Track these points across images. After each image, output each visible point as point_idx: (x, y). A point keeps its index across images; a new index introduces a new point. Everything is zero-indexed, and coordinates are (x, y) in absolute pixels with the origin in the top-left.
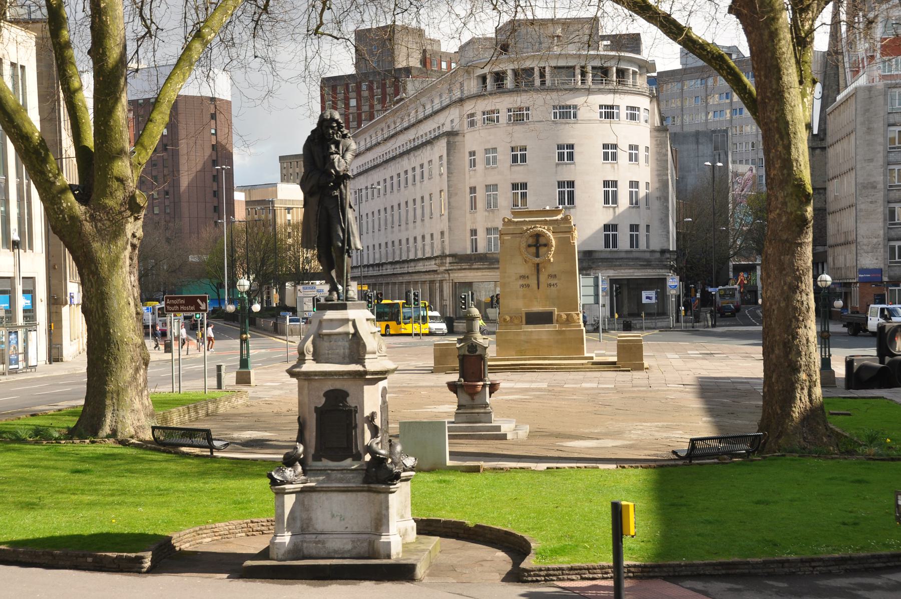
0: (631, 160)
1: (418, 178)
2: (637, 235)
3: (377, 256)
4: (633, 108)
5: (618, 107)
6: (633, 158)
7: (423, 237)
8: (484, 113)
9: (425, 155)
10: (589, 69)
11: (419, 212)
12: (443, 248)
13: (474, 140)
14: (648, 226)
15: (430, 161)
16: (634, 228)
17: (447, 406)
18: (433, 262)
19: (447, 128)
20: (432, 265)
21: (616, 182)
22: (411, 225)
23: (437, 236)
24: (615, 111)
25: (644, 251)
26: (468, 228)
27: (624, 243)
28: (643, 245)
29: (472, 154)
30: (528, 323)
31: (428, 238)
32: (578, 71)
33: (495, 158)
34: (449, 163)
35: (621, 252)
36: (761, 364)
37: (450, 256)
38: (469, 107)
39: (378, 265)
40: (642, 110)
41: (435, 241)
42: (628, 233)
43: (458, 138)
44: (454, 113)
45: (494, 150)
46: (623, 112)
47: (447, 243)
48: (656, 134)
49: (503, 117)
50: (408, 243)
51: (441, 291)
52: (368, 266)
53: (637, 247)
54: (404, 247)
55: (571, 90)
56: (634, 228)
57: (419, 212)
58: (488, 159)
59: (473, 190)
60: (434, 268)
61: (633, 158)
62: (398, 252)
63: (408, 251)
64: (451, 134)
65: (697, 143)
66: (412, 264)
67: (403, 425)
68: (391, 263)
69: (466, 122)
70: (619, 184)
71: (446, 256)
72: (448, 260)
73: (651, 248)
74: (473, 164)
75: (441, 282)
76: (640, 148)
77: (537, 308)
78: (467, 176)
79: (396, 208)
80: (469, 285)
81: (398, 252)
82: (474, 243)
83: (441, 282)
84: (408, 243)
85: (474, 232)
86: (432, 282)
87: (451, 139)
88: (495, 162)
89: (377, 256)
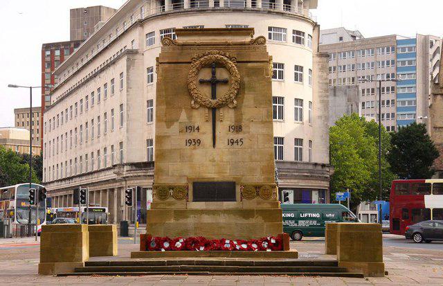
0: (296, 79)
1: (102, 97)
2: (301, 149)
3: (68, 171)
4: (298, 32)
5: (285, 30)
6: (298, 78)
7: (105, 149)
11: (102, 127)
12: (122, 158)
14: (310, 141)
15: (112, 81)
16: (299, 141)
18: (112, 171)
19: (129, 47)
20: (110, 175)
21: (283, 98)
22: (96, 140)
23: (117, 147)
24: (283, 33)
25: (307, 164)
27: (289, 155)
28: (306, 159)
30: (197, 198)
31: (109, 149)
34: (128, 79)
35: (287, 162)
36: (384, 248)
37: (126, 164)
38: (149, 28)
40: (306, 35)
42: (293, 146)
43: (137, 57)
46: (290, 35)
47: (124, 153)
48: (318, 59)
50: (92, 157)
51: (119, 198)
52: (61, 180)
53: (301, 160)
55: (241, 11)
56: (299, 141)
57: (102, 127)
60: (114, 176)
61: (298, 78)
62: (84, 165)
63: (93, 164)
64: (131, 53)
65: (335, 95)
66: (96, 175)
69: (145, 40)
70: (285, 100)
71: (124, 165)
72: (126, 168)
73: (314, 161)
75: (120, 189)
76: (304, 69)
78: (145, 91)
80: (328, 253)
81: (84, 165)
83: (112, 190)
84: (92, 157)
86: (112, 190)
87: (131, 57)
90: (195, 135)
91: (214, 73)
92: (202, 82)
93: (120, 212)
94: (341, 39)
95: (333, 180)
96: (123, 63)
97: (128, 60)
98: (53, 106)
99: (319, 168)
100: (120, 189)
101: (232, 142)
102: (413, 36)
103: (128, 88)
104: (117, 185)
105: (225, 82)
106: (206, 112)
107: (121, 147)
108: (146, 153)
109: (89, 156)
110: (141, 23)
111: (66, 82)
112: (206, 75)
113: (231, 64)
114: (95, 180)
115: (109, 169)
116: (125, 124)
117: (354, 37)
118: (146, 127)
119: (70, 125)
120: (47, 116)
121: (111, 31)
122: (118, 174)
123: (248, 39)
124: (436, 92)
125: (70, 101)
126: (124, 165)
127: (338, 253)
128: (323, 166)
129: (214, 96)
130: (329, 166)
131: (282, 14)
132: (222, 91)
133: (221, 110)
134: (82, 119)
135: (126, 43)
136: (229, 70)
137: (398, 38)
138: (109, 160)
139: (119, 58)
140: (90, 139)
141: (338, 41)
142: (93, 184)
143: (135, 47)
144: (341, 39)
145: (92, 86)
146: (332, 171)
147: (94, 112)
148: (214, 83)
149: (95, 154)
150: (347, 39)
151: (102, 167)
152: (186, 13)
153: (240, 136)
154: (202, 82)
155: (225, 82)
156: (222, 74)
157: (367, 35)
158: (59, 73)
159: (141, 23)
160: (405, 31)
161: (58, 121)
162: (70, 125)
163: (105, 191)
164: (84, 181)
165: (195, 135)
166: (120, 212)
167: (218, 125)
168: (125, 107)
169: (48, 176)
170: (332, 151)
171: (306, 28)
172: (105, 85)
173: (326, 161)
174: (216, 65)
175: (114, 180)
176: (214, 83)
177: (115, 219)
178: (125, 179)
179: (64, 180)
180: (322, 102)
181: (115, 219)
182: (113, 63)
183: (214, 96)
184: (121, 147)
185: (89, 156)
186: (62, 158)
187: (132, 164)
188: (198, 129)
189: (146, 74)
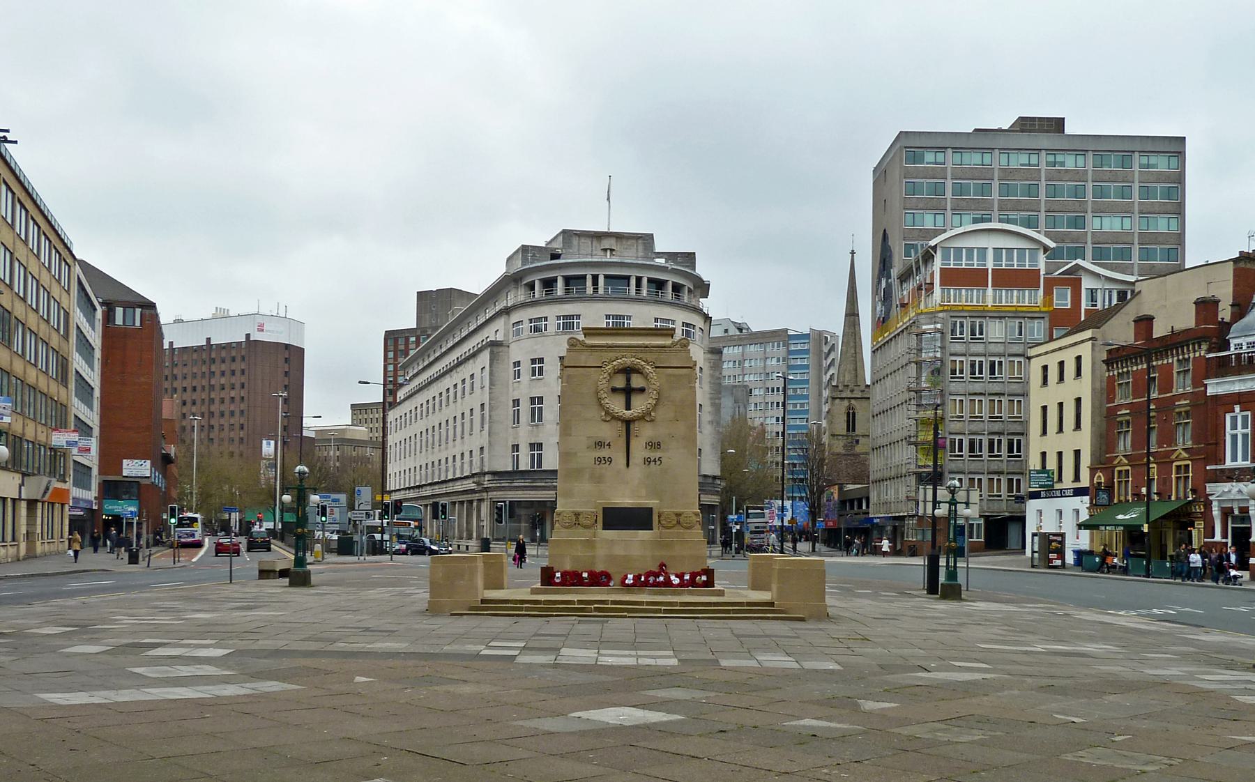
3: (418, 478)
4: (688, 325)
5: (673, 322)
8: (531, 321)
9: (465, 372)
10: (645, 281)
13: (521, 351)
15: (472, 376)
17: (1088, 618)
18: (471, 481)
19: (492, 338)
23: (476, 453)
26: (510, 444)
29: (517, 364)
30: (607, 526)
31: (467, 455)
32: (633, 282)
33: (541, 369)
34: (491, 374)
38: (515, 317)
39: (418, 487)
41: (474, 459)
43: (501, 349)
44: (500, 324)
45: (541, 360)
47: (486, 460)
48: (709, 356)
49: (552, 325)
54: (443, 467)
58: (534, 370)
59: (516, 402)
60: (473, 486)
62: (437, 472)
63: (447, 471)
64: (495, 344)
67: (564, 574)
68: (430, 484)
71: (485, 474)
74: (518, 375)
75: (480, 501)
77: (624, 499)
79: (437, 428)
81: (437, 472)
82: (516, 460)
83: (471, 502)
85: (516, 448)
86: (471, 502)
87: (495, 349)
88: (541, 373)
89: (418, 478)
90: (604, 453)
91: (628, 380)
92: (614, 390)
93: (480, 528)
94: (726, 331)
95: (727, 493)
96: (485, 357)
97: (492, 353)
98: (400, 403)
99: (710, 480)
100: (480, 501)
101: (648, 461)
102: (807, 331)
103: (492, 384)
104: (477, 496)
105: (642, 390)
106: (620, 427)
107: (482, 453)
108: (510, 460)
109: (443, 462)
110: (507, 311)
111: (415, 376)
112: (620, 382)
113: (649, 369)
114: (450, 490)
115: (467, 477)
116: (486, 427)
117: (741, 330)
118: (511, 430)
119: (420, 426)
120: (392, 415)
121: (470, 319)
122: (478, 484)
123: (668, 342)
124: (835, 395)
125: (420, 399)
126: (485, 474)
127: (774, 587)
128: (714, 478)
129: (628, 407)
130: (720, 478)
131: (669, 304)
132: (640, 404)
133: (637, 424)
134: (434, 420)
135: (489, 334)
136: (645, 376)
137: (790, 333)
138: (466, 467)
139: (480, 350)
140: (443, 442)
141: (722, 334)
142: (447, 494)
143: (500, 337)
144: (726, 331)
145: (447, 382)
146: (723, 484)
147: (448, 412)
148: (628, 392)
149: (450, 460)
150: (733, 331)
151: (458, 475)
152: (561, 300)
153: (657, 454)
154: (614, 390)
155: (642, 390)
156: (637, 381)
157: (755, 328)
158: (405, 367)
159: (507, 311)
160: (799, 326)
161: (404, 422)
162: (420, 426)
163: (462, 503)
164: (437, 490)
165: (604, 453)
166: (480, 528)
167: (633, 442)
168: (487, 407)
169: (391, 484)
170: (724, 457)
171: (697, 321)
172: (463, 381)
173: (718, 473)
174: (628, 371)
175: (473, 491)
176: (628, 392)
177: (475, 535)
178: (487, 490)
179: (413, 488)
180: (713, 405)
181: (475, 535)
182: (474, 355)
183: (628, 407)
184: (482, 453)
185: (443, 462)
186: (410, 463)
187: (494, 473)
188: (609, 445)
189: (512, 369)
